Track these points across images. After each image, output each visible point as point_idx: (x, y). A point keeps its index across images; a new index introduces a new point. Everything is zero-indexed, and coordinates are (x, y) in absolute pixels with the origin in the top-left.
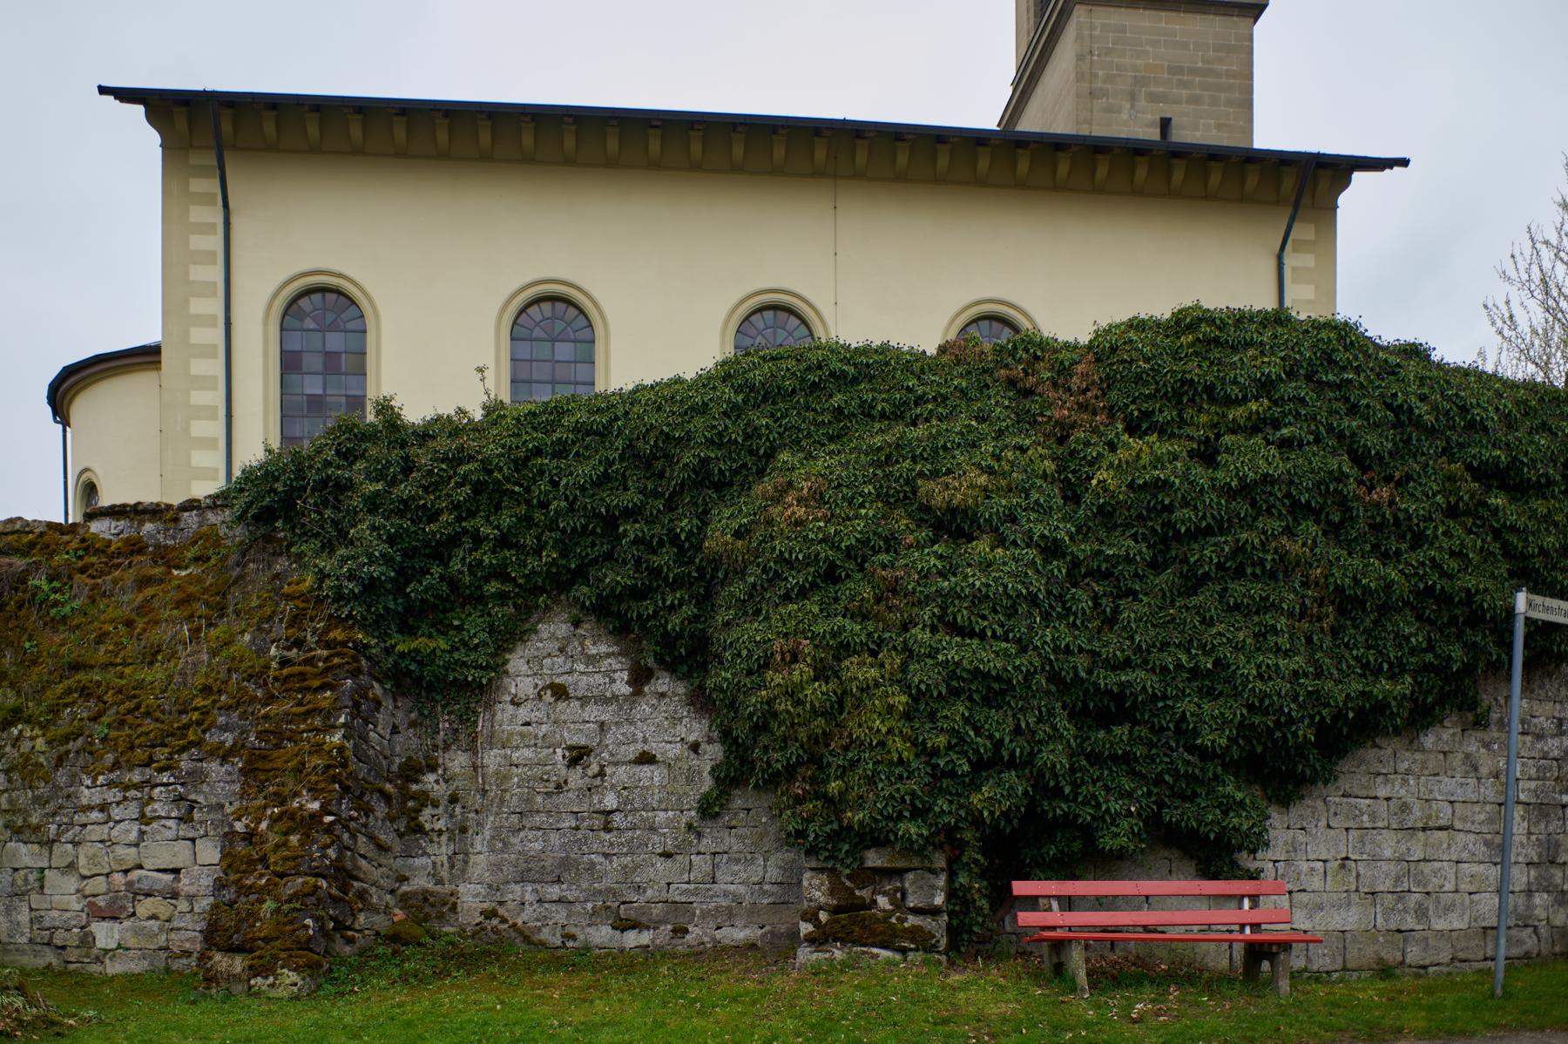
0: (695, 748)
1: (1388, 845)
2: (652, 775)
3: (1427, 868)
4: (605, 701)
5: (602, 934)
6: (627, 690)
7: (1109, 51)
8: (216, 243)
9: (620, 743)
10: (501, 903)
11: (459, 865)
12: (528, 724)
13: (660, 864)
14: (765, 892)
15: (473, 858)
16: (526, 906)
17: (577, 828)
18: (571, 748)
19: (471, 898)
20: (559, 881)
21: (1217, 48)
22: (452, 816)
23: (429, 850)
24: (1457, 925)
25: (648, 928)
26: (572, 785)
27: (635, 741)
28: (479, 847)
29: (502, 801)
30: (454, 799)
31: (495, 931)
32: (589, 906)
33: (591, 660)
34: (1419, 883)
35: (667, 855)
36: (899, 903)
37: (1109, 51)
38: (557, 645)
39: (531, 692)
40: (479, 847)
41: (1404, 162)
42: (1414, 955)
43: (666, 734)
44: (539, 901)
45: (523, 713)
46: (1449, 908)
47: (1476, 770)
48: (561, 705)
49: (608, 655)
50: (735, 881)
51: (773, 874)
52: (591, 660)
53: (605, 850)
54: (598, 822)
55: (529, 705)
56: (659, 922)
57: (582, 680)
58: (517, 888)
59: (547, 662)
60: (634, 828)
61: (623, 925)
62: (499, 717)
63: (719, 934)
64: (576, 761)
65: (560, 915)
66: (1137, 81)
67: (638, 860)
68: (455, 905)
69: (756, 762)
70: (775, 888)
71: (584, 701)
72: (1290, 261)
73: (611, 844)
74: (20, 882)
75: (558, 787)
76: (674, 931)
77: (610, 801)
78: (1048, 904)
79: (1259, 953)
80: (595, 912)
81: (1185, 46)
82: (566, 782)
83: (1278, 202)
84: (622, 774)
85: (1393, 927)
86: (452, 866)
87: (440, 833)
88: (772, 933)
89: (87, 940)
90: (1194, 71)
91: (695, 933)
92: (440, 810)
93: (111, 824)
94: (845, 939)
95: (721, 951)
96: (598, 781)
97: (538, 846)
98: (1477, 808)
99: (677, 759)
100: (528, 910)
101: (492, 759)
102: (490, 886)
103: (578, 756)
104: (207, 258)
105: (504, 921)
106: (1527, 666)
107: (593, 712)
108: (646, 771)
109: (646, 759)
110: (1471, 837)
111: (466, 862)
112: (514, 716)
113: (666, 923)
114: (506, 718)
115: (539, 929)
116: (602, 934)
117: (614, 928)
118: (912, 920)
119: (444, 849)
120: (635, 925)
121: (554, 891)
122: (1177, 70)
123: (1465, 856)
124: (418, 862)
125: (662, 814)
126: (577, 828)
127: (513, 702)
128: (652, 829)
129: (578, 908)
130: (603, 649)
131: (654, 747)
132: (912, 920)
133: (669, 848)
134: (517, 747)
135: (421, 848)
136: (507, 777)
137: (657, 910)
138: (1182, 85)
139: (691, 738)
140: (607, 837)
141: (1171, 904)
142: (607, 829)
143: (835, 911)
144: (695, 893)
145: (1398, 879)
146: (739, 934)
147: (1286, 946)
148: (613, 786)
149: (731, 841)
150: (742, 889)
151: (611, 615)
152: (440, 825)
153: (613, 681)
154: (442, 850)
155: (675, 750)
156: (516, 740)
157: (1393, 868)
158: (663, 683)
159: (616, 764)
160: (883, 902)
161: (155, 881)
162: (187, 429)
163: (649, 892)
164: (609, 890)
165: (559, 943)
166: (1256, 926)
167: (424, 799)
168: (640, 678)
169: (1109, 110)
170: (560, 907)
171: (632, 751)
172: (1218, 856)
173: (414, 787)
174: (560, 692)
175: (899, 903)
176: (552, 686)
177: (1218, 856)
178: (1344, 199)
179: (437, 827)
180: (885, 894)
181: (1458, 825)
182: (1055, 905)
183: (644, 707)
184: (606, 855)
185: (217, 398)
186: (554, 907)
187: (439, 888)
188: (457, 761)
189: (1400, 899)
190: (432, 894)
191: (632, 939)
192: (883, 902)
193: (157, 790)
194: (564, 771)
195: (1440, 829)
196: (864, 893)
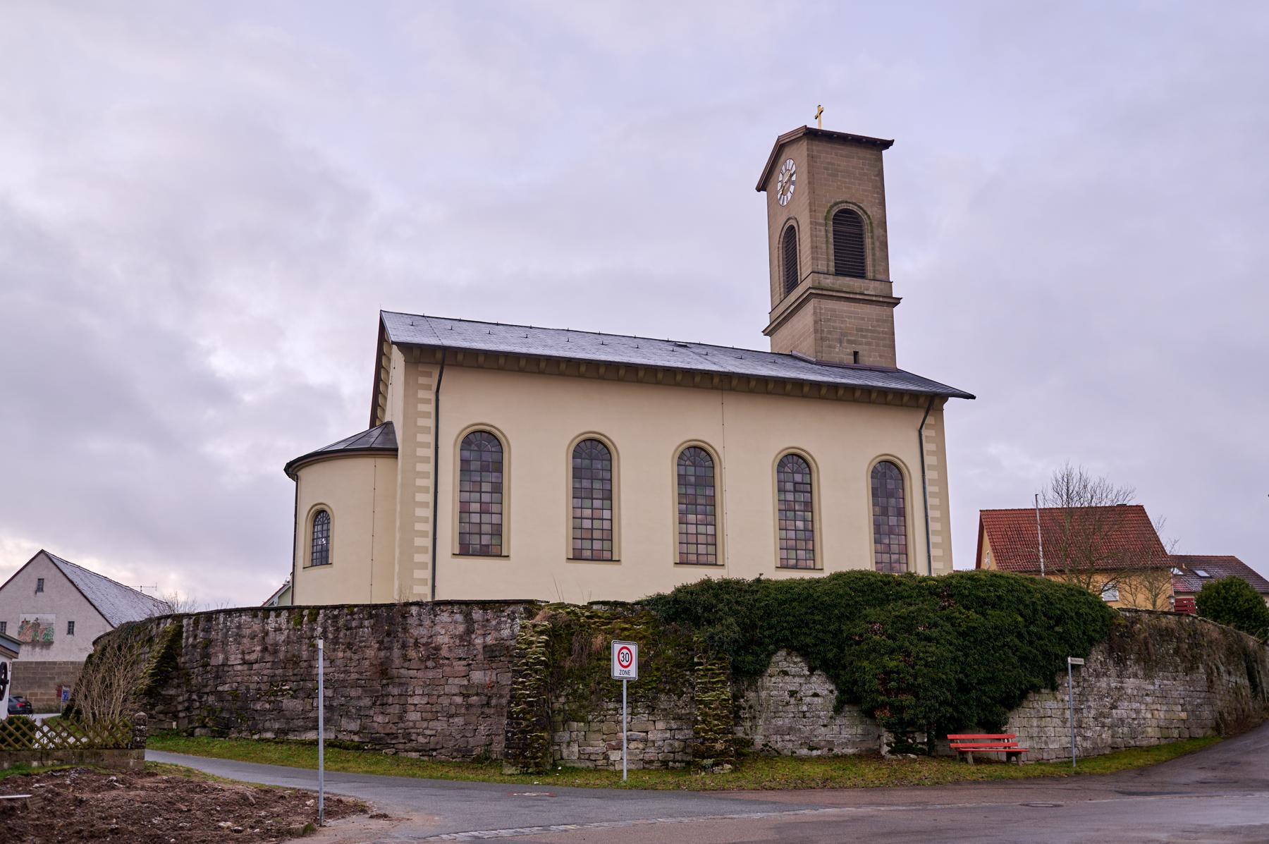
0: (831, 692)
2: (819, 700)
4: (800, 676)
7: (829, 320)
8: (431, 408)
9: (807, 690)
16: (778, 742)
19: (759, 740)
21: (878, 321)
33: (795, 663)
35: (825, 726)
37: (829, 320)
41: (973, 397)
42: (1045, 756)
43: (820, 688)
50: (846, 734)
51: (860, 731)
52: (795, 663)
57: (793, 669)
61: (811, 749)
65: (790, 745)
69: (849, 697)
71: (794, 676)
72: (924, 433)
77: (805, 708)
78: (961, 741)
79: (1010, 754)
81: (863, 319)
89: (606, 758)
90: (867, 330)
91: (836, 750)
94: (901, 752)
95: (844, 756)
101: (763, 694)
103: (792, 694)
107: (797, 680)
108: (816, 699)
109: (816, 695)
114: (767, 682)
120: (817, 749)
121: (787, 737)
131: (818, 691)
141: (979, 741)
146: (850, 751)
147: (1019, 753)
149: (845, 721)
151: (804, 652)
162: (414, 497)
167: (740, 707)
168: (812, 670)
171: (811, 692)
172: (993, 726)
174: (786, 673)
177: (993, 726)
178: (945, 406)
183: (814, 679)
185: (430, 483)
191: (815, 753)
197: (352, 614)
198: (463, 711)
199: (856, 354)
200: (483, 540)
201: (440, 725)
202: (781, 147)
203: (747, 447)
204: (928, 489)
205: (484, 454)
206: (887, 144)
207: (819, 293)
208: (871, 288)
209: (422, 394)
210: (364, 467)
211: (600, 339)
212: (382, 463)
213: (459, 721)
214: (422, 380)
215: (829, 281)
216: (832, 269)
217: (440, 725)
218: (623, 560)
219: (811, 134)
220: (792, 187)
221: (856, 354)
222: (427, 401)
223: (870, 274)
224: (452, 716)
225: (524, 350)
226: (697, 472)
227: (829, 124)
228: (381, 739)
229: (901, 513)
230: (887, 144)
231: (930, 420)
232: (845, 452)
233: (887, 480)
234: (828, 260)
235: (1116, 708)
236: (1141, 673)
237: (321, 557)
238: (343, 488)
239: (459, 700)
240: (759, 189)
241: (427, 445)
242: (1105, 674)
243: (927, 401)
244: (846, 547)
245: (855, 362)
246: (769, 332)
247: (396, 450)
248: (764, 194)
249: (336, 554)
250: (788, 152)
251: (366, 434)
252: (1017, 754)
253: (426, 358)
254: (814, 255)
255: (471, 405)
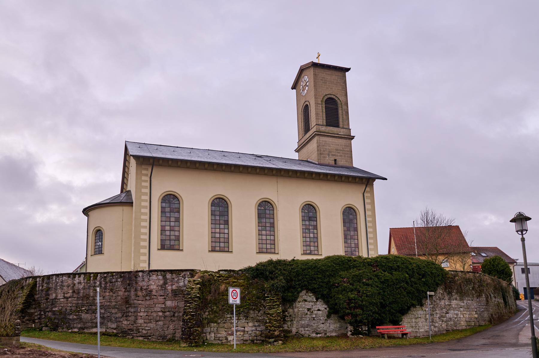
0: (326, 308)
4: (312, 302)
5: (314, 335)
7: (323, 146)
9: (315, 308)
16: (302, 331)
19: (294, 330)
21: (345, 146)
30: (290, 316)
33: (310, 296)
35: (323, 324)
36: (362, 329)
37: (323, 146)
41: (386, 179)
42: (418, 335)
43: (321, 307)
45: (300, 303)
50: (332, 327)
51: (338, 326)
52: (310, 296)
57: (309, 299)
64: (310, 311)
65: (308, 332)
66: (330, 152)
69: (334, 311)
71: (309, 302)
72: (365, 195)
77: (314, 316)
79: (403, 334)
81: (338, 145)
83: (363, 183)
84: (316, 312)
89: (227, 339)
91: (328, 334)
95: (331, 337)
101: (296, 310)
103: (309, 310)
104: (146, 187)
107: (311, 303)
109: (319, 310)
114: (298, 304)
116: (314, 335)
120: (320, 334)
121: (307, 329)
122: (336, 150)
130: (311, 295)
131: (320, 308)
137: (322, 331)
138: (338, 153)
141: (390, 329)
146: (334, 334)
149: (331, 321)
151: (314, 291)
154: (289, 323)
155: (323, 309)
167: (286, 316)
168: (317, 299)
169: (324, 157)
171: (317, 309)
172: (396, 322)
174: (306, 301)
177: (396, 322)
178: (374, 183)
183: (318, 303)
188: (291, 310)
191: (319, 335)
197: (113, 276)
198: (163, 319)
199: (335, 160)
200: (171, 242)
201: (152, 325)
202: (302, 71)
203: (289, 202)
204: (367, 219)
205: (171, 202)
206: (348, 70)
207: (319, 134)
208: (342, 132)
209: (144, 178)
210: (118, 211)
211: (223, 154)
212: (126, 209)
213: (161, 323)
214: (144, 172)
215: (323, 129)
216: (325, 123)
217: (152, 325)
218: (233, 251)
219: (315, 65)
220: (307, 88)
221: (335, 160)
222: (146, 181)
223: (341, 126)
224: (158, 321)
225: (189, 159)
226: (266, 211)
227: (322, 61)
228: (126, 331)
229: (356, 230)
230: (348, 70)
231: (368, 189)
232: (331, 203)
233: (349, 215)
234: (323, 119)
235: (448, 313)
236: (458, 298)
237: (99, 251)
238: (108, 220)
239: (161, 314)
240: (292, 89)
241: (146, 201)
242: (443, 299)
243: (366, 180)
244: (332, 244)
245: (335, 164)
246: (297, 151)
247: (132, 203)
248: (295, 91)
249: (105, 249)
250: (305, 72)
251: (119, 196)
252: (406, 334)
253: (145, 162)
254: (317, 117)
255: (165, 183)
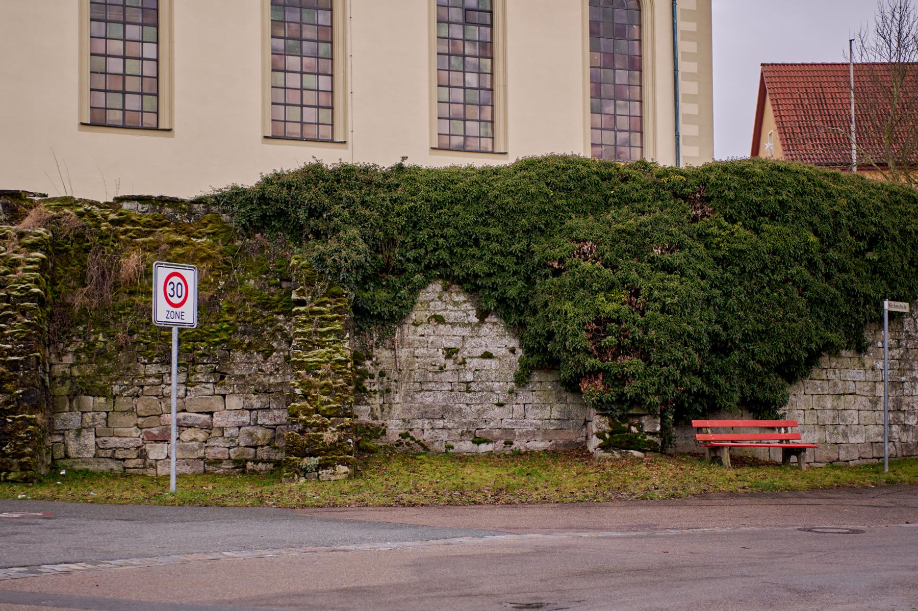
0: (513, 351)
1: (829, 402)
3: (846, 413)
4: (465, 325)
5: (467, 446)
6: (476, 320)
9: (474, 347)
10: (411, 430)
11: (386, 410)
12: (423, 336)
13: (497, 409)
14: (551, 424)
15: (394, 407)
16: (424, 431)
17: (452, 391)
18: (447, 349)
19: (394, 428)
20: (443, 418)
22: (381, 383)
23: (369, 401)
24: (860, 441)
25: (492, 442)
26: (448, 368)
27: (482, 346)
28: (397, 400)
29: (410, 376)
31: (408, 444)
32: (460, 431)
33: (456, 304)
34: (843, 420)
35: (500, 405)
38: (437, 295)
39: (425, 320)
40: (397, 400)
42: (843, 455)
43: (497, 342)
44: (433, 428)
45: (420, 330)
46: (857, 432)
47: (864, 365)
48: (441, 327)
49: (465, 302)
50: (535, 418)
52: (456, 304)
53: (468, 402)
54: (463, 387)
55: (424, 326)
56: (498, 439)
57: (452, 314)
58: (420, 421)
59: (432, 304)
60: (482, 391)
62: (406, 331)
63: (528, 445)
65: (444, 435)
67: (485, 407)
68: (384, 431)
69: (542, 358)
70: (556, 422)
71: (453, 325)
73: (471, 399)
74: (88, 420)
75: (441, 368)
76: (506, 443)
77: (469, 377)
78: (712, 429)
79: (788, 452)
80: (462, 434)
82: (445, 366)
84: (474, 363)
85: (833, 441)
86: (382, 410)
87: (375, 392)
88: (556, 444)
91: (516, 444)
92: (375, 380)
93: (163, 386)
96: (462, 367)
97: (431, 399)
98: (865, 384)
99: (504, 356)
100: (426, 433)
102: (404, 420)
103: (450, 353)
105: (413, 439)
106: (889, 320)
107: (458, 331)
109: (487, 356)
110: (864, 398)
111: (390, 408)
112: (415, 331)
113: (501, 439)
115: (433, 443)
116: (467, 446)
117: (474, 442)
118: (649, 438)
119: (378, 401)
120: (487, 441)
121: (440, 423)
123: (861, 407)
124: (363, 408)
125: (497, 384)
126: (452, 391)
127: (413, 324)
128: (492, 391)
129: (454, 432)
131: (492, 350)
132: (649, 438)
133: (501, 401)
134: (417, 348)
135: (364, 400)
136: (413, 363)
139: (511, 346)
140: (468, 395)
142: (468, 390)
143: (611, 433)
144: (516, 424)
145: (834, 418)
146: (539, 445)
148: (470, 369)
149: (532, 398)
150: (540, 422)
151: (470, 285)
152: (376, 387)
153: (468, 315)
154: (377, 401)
155: (504, 351)
156: (417, 344)
157: (831, 413)
158: (492, 319)
159: (472, 358)
160: (634, 429)
161: (196, 419)
163: (492, 424)
164: (470, 422)
165: (444, 451)
166: (787, 441)
167: (365, 374)
168: (483, 315)
170: (444, 431)
171: (480, 351)
173: (359, 367)
175: (640, 430)
176: (435, 316)
177: (763, 407)
179: (373, 389)
180: (635, 426)
181: (858, 393)
182: (709, 431)
183: (485, 329)
184: (467, 405)
186: (440, 432)
187: (375, 422)
188: (383, 354)
189: (835, 428)
190: (371, 425)
191: (484, 448)
192: (634, 429)
193: (199, 367)
194: (443, 361)
195: (850, 394)
196: (626, 425)
